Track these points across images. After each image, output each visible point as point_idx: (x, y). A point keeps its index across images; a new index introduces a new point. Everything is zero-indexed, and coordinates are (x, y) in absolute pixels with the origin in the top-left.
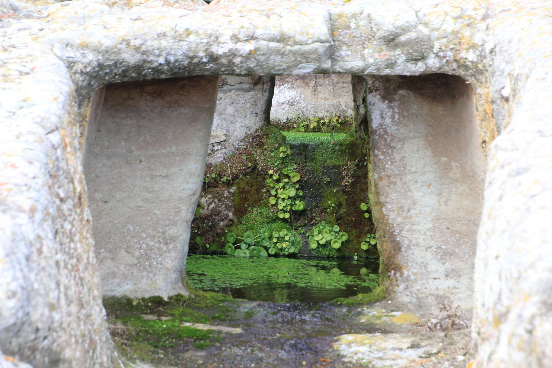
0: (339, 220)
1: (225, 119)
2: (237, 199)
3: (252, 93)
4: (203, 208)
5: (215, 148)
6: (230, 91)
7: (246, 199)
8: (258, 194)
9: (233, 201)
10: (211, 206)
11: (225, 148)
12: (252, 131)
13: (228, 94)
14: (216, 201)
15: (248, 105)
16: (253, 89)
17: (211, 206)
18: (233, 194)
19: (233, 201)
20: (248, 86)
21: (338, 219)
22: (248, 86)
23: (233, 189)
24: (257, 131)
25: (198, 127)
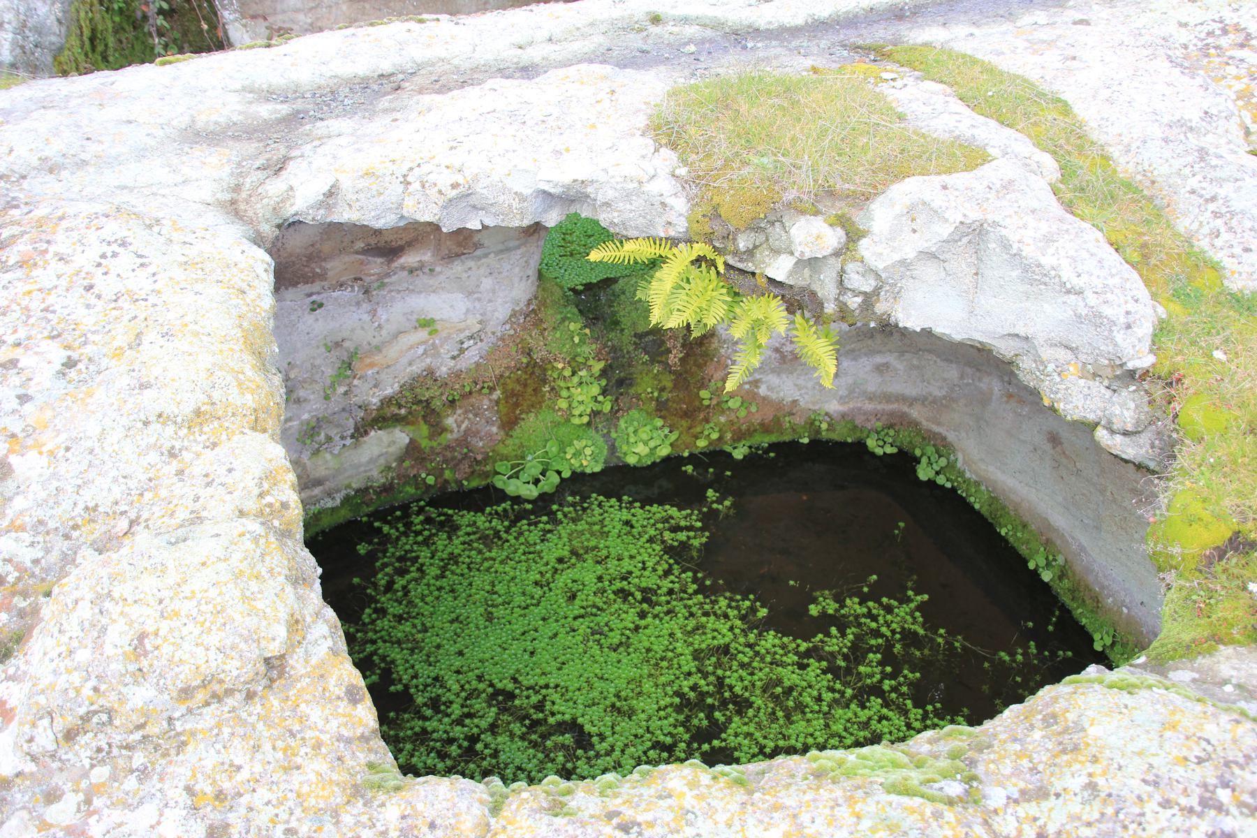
0: (662, 408)
1: (479, 299)
2: (503, 408)
3: (523, 249)
4: (452, 432)
5: (465, 346)
6: (486, 256)
7: (517, 405)
8: (536, 395)
9: (498, 411)
10: (464, 426)
11: (481, 340)
12: (522, 305)
13: (484, 260)
14: (471, 416)
15: (517, 270)
16: (524, 244)
17: (464, 426)
18: (497, 402)
19: (498, 411)
20: (517, 243)
21: (658, 409)
22: (517, 243)
23: (497, 394)
24: (529, 303)
25: (514, 807)
